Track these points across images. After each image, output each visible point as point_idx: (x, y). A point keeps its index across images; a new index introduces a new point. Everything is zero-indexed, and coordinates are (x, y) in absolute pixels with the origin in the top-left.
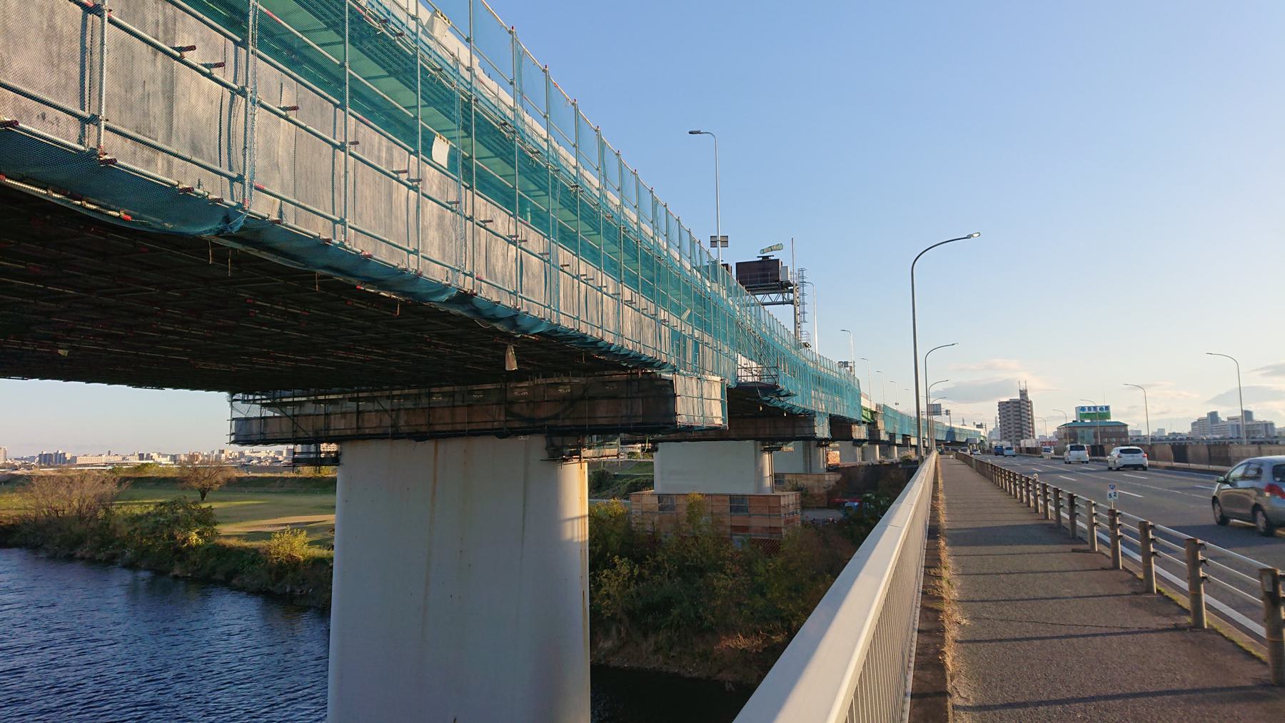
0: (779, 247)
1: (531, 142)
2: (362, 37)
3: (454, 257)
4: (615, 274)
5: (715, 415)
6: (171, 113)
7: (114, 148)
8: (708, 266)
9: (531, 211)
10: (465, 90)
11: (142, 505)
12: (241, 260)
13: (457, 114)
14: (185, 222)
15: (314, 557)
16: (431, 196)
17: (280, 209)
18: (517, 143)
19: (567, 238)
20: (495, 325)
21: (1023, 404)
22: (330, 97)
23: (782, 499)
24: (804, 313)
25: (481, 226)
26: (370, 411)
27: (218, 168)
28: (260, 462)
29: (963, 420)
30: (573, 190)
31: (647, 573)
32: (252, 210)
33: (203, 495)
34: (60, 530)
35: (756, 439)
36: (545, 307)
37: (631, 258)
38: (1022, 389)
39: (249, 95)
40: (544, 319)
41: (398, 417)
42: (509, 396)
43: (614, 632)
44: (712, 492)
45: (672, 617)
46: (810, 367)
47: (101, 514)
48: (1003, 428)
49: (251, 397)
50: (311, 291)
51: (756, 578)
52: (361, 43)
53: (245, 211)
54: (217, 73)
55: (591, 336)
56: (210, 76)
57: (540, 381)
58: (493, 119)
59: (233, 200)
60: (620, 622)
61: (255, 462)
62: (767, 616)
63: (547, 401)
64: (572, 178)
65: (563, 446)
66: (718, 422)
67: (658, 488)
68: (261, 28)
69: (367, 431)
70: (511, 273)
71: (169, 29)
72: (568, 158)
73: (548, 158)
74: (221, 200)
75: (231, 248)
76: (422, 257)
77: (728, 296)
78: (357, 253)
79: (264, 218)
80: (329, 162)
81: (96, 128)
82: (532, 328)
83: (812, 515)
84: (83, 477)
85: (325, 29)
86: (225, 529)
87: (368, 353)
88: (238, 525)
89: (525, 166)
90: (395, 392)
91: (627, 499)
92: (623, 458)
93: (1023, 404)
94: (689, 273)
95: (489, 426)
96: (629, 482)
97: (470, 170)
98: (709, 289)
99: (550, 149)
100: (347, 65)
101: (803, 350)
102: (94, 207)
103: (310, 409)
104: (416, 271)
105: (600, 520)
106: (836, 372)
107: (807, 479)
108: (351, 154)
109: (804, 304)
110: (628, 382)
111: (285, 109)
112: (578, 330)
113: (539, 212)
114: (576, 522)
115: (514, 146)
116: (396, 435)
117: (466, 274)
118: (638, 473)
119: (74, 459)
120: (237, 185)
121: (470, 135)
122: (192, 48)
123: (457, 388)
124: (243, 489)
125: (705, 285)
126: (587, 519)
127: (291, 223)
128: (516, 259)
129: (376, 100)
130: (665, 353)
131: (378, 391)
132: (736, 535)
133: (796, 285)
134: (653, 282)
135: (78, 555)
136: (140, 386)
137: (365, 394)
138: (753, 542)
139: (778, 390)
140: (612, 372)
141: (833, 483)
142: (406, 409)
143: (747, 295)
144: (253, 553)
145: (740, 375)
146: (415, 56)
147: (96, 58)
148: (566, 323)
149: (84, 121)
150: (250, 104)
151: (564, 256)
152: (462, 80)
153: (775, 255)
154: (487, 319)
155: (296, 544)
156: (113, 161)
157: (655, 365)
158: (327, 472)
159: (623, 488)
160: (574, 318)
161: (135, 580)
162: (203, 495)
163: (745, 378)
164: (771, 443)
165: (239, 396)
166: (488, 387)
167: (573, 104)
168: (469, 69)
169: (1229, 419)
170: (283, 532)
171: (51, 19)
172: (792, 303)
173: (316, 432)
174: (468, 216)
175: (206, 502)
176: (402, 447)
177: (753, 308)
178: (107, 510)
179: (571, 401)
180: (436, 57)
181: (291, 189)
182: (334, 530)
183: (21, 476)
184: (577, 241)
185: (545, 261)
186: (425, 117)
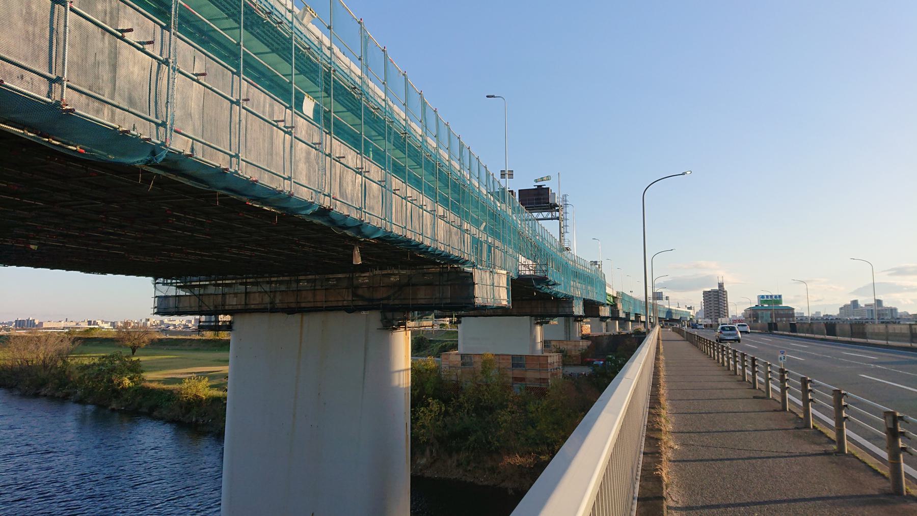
0: (548, 178)
1: (374, 101)
4: (432, 196)
5: (502, 298)
7: (72, 100)
11: (90, 358)
12: (160, 182)
13: (321, 79)
14: (123, 155)
18: (363, 102)
19: (398, 170)
20: (345, 231)
21: (720, 293)
22: (229, 67)
23: (549, 358)
24: (566, 226)
25: (337, 161)
27: (147, 116)
29: (678, 304)
32: (171, 147)
35: (531, 316)
36: (382, 219)
38: (720, 282)
39: (171, 65)
41: (275, 296)
42: (355, 282)
43: (428, 452)
48: (706, 304)
49: (169, 281)
52: (252, 29)
54: (148, 48)
55: (415, 240)
56: (143, 51)
57: (378, 272)
58: (346, 84)
59: (158, 140)
61: (171, 328)
63: (383, 287)
64: (403, 127)
67: (461, 349)
68: (181, 17)
69: (253, 306)
71: (114, 16)
72: (400, 113)
74: (149, 140)
76: (294, 182)
78: (247, 179)
79: (180, 153)
80: (227, 113)
82: (372, 234)
83: (570, 370)
84: (48, 336)
85: (227, 18)
86: (149, 376)
87: (254, 250)
90: (273, 279)
91: (439, 357)
92: (437, 328)
93: (720, 293)
94: (485, 197)
95: (340, 304)
97: (329, 120)
98: (499, 209)
99: (387, 106)
103: (211, 290)
104: (289, 192)
107: (567, 345)
108: (244, 108)
109: (566, 219)
110: (441, 274)
111: (197, 75)
112: (405, 236)
115: (361, 104)
117: (325, 195)
119: (41, 324)
120: (162, 129)
121: (329, 95)
122: (130, 30)
123: (317, 277)
124: (162, 347)
125: (496, 205)
126: (410, 371)
127: (200, 157)
128: (362, 185)
130: (467, 253)
131: (260, 278)
132: (516, 384)
133: (561, 206)
134: (459, 201)
135: (43, 393)
137: (251, 280)
138: (527, 388)
139: (547, 280)
140: (429, 267)
141: (585, 347)
144: (169, 393)
146: (291, 38)
148: (397, 231)
149: (51, 81)
150: (171, 71)
151: (396, 183)
152: (324, 57)
153: (546, 184)
154: (340, 227)
155: (200, 387)
156: (72, 110)
158: (224, 335)
159: (436, 350)
163: (524, 272)
164: (542, 318)
166: (340, 276)
168: (330, 49)
169: (866, 305)
172: (558, 218)
173: (216, 307)
174: (327, 153)
175: (136, 356)
176: (279, 318)
177: (530, 222)
178: (64, 361)
180: (306, 40)
181: (200, 133)
182: (227, 377)
186: (297, 82)
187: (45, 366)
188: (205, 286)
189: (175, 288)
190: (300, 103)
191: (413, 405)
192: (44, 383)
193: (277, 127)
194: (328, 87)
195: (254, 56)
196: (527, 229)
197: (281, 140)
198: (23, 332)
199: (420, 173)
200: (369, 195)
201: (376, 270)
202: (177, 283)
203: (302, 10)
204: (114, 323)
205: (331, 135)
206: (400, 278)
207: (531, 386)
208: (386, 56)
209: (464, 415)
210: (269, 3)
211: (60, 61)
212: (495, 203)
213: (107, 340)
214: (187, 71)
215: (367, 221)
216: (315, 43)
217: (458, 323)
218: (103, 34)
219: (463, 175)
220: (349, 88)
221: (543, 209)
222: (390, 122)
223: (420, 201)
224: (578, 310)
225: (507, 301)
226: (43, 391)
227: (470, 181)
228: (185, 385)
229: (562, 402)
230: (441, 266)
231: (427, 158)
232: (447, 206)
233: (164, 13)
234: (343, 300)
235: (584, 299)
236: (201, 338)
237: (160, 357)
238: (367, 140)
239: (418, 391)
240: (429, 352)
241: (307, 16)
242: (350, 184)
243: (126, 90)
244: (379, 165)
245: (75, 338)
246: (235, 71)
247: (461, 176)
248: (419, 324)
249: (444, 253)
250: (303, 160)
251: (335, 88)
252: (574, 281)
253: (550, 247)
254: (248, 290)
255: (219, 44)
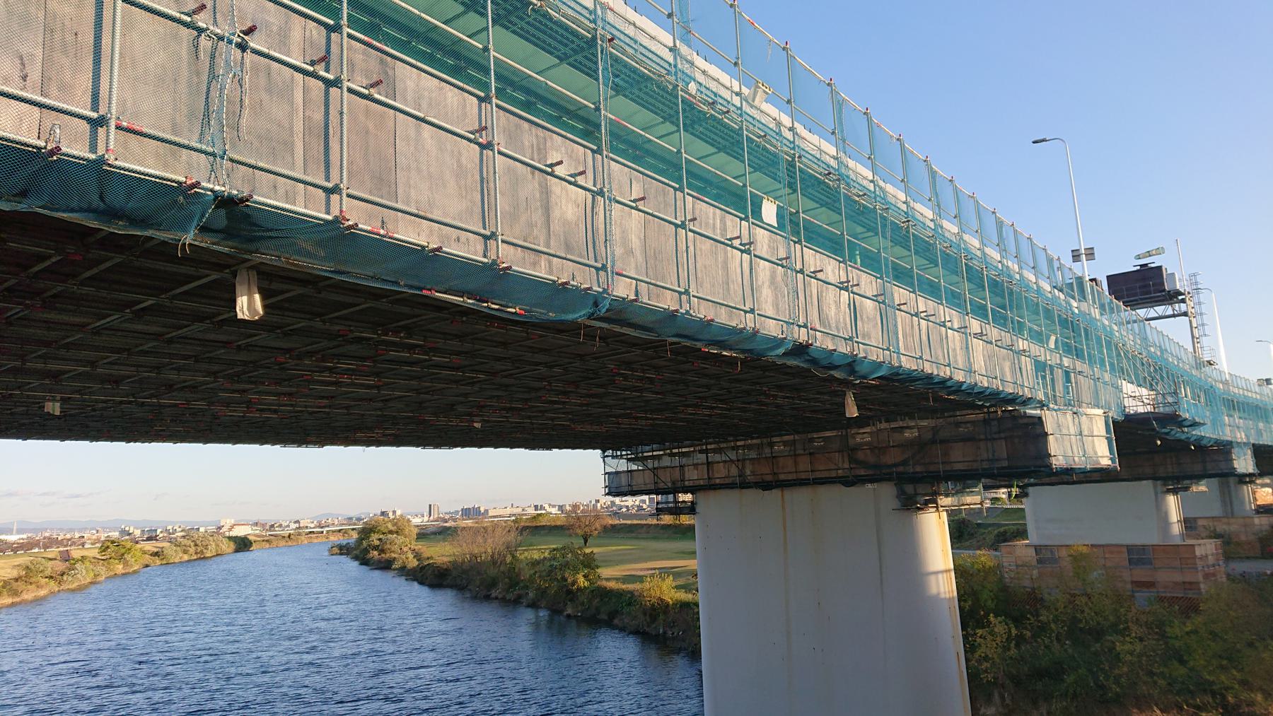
0: (1159, 251)
1: (857, 186)
2: (693, 122)
3: (787, 312)
4: (958, 306)
5: (1100, 454)
6: (548, 221)
7: (509, 257)
8: (1072, 283)
9: (860, 254)
10: (789, 150)
11: (538, 551)
12: (606, 337)
13: (782, 173)
14: (564, 312)
15: (681, 601)
16: (762, 256)
17: (636, 288)
18: (842, 190)
19: (902, 276)
20: (832, 372)
22: (671, 183)
23: (1196, 548)
24: (1203, 325)
25: (811, 277)
26: (719, 462)
27: (586, 261)
28: (628, 510)
30: (905, 225)
31: (1029, 634)
32: (614, 293)
33: (586, 541)
34: (479, 573)
35: (1154, 478)
36: (883, 349)
37: (975, 287)
39: (606, 194)
40: (884, 362)
41: (744, 467)
42: (851, 442)
43: (996, 697)
44: (1103, 543)
45: (1065, 685)
46: (1219, 389)
47: (509, 559)
49: (619, 453)
50: (664, 357)
51: (1172, 642)
52: (693, 128)
53: (609, 295)
54: (581, 180)
55: (938, 375)
56: (575, 184)
57: (884, 425)
58: (816, 171)
59: (599, 287)
60: (1003, 688)
61: (624, 510)
62: (1191, 687)
63: (893, 446)
64: (903, 214)
65: (916, 494)
66: (1105, 462)
67: (1034, 537)
68: (612, 134)
69: (718, 481)
70: (844, 319)
71: (541, 151)
72: (897, 194)
73: (875, 198)
74: (589, 289)
75: (600, 328)
76: (758, 314)
77: (1102, 314)
78: (701, 319)
79: (624, 299)
80: (672, 241)
81: (495, 242)
82: (873, 373)
83: (1240, 567)
84: (495, 526)
85: (662, 123)
86: (605, 572)
87: (713, 408)
88: (618, 567)
89: (851, 210)
90: (739, 443)
91: (996, 550)
92: (988, 504)
94: (1050, 295)
95: (833, 474)
96: (996, 532)
97: (798, 224)
98: (1076, 311)
99: (877, 189)
100: (683, 151)
101: (1208, 369)
102: (497, 307)
103: (666, 461)
104: (753, 329)
105: (965, 572)
106: (1256, 392)
107: (1228, 524)
108: (690, 230)
109: (1201, 314)
110: (986, 422)
111: (634, 201)
112: (922, 371)
113: (869, 254)
114: (940, 576)
115: (839, 193)
116: (743, 484)
117: (800, 326)
118: (1007, 520)
119: (487, 511)
120: (602, 273)
121: (795, 191)
122: (560, 163)
123: (796, 437)
124: (617, 535)
125: (1070, 305)
126: (953, 574)
127: (645, 300)
128: (849, 305)
129: (709, 176)
130: (1024, 383)
131: (723, 442)
132: (1138, 592)
133: (1189, 293)
134: (1004, 308)
135: (493, 595)
136: (533, 448)
137: (713, 446)
138: (1161, 599)
139: (1180, 419)
140: (964, 412)
141: (1267, 528)
142: (750, 459)
143: (1125, 311)
144: (629, 595)
145: (1127, 405)
146: (741, 128)
147: (492, 185)
148: (907, 364)
149: (486, 238)
150: (607, 201)
151: (900, 294)
152: (785, 141)
153: (1155, 261)
154: (824, 367)
155: (664, 587)
156: (509, 268)
157: (1017, 401)
158: (685, 520)
159: (990, 538)
160: (917, 358)
161: (537, 617)
162: (586, 541)
163: (1135, 408)
164: (1177, 482)
165: (609, 452)
166: (828, 434)
167: (898, 139)
168: (791, 129)
170: (652, 575)
171: (459, 161)
172: (1185, 314)
173: (673, 483)
174: (798, 269)
175: (589, 547)
176: (752, 495)
177: (1136, 325)
178: (513, 557)
179: (919, 445)
180: (760, 126)
181: (644, 271)
182: (696, 575)
183: (450, 528)
184: (912, 277)
185: (879, 302)
186: (752, 182)
187: (494, 562)
188: (659, 457)
189: (625, 461)
190: (757, 210)
191: (964, 627)
192: (493, 584)
193: (732, 246)
194: (792, 181)
195: (696, 161)
196: (1131, 337)
197: (738, 260)
198: (469, 523)
199: (939, 275)
200: (861, 316)
201: (881, 423)
202: (627, 455)
203: (753, 89)
204: (562, 506)
205: (801, 244)
206: (919, 431)
207: (1168, 595)
208: (869, 120)
209: (1052, 642)
210: (712, 91)
211: (492, 214)
212: (1068, 303)
213: (556, 527)
214: (624, 198)
215: (862, 355)
216: (771, 126)
217: (1023, 497)
218: (533, 174)
219: (1008, 267)
220: (820, 174)
221: (1157, 301)
222: (883, 209)
223: (939, 315)
224: (1244, 463)
225: (1111, 459)
226: (494, 594)
227: (1021, 275)
228: (647, 585)
229: (1231, 621)
230: (986, 410)
231: (945, 251)
232: (986, 316)
233: (592, 133)
234: (836, 467)
235: (1253, 445)
236: (659, 522)
237: (614, 548)
238: (851, 241)
239: (970, 603)
240: (978, 542)
241: (760, 93)
242: (833, 308)
243: (562, 233)
244: (735, 212)
245: (524, 527)
246: (677, 186)
247: (1005, 269)
248: (959, 500)
249: (989, 391)
250: (767, 284)
251: (802, 180)
252: (1230, 416)
253: (1178, 362)
254: (710, 460)
255: (654, 156)
